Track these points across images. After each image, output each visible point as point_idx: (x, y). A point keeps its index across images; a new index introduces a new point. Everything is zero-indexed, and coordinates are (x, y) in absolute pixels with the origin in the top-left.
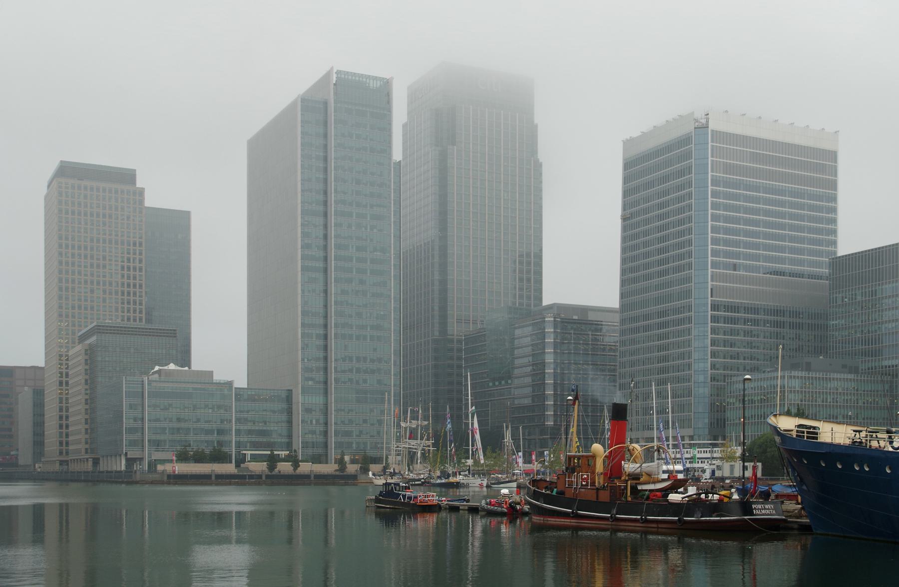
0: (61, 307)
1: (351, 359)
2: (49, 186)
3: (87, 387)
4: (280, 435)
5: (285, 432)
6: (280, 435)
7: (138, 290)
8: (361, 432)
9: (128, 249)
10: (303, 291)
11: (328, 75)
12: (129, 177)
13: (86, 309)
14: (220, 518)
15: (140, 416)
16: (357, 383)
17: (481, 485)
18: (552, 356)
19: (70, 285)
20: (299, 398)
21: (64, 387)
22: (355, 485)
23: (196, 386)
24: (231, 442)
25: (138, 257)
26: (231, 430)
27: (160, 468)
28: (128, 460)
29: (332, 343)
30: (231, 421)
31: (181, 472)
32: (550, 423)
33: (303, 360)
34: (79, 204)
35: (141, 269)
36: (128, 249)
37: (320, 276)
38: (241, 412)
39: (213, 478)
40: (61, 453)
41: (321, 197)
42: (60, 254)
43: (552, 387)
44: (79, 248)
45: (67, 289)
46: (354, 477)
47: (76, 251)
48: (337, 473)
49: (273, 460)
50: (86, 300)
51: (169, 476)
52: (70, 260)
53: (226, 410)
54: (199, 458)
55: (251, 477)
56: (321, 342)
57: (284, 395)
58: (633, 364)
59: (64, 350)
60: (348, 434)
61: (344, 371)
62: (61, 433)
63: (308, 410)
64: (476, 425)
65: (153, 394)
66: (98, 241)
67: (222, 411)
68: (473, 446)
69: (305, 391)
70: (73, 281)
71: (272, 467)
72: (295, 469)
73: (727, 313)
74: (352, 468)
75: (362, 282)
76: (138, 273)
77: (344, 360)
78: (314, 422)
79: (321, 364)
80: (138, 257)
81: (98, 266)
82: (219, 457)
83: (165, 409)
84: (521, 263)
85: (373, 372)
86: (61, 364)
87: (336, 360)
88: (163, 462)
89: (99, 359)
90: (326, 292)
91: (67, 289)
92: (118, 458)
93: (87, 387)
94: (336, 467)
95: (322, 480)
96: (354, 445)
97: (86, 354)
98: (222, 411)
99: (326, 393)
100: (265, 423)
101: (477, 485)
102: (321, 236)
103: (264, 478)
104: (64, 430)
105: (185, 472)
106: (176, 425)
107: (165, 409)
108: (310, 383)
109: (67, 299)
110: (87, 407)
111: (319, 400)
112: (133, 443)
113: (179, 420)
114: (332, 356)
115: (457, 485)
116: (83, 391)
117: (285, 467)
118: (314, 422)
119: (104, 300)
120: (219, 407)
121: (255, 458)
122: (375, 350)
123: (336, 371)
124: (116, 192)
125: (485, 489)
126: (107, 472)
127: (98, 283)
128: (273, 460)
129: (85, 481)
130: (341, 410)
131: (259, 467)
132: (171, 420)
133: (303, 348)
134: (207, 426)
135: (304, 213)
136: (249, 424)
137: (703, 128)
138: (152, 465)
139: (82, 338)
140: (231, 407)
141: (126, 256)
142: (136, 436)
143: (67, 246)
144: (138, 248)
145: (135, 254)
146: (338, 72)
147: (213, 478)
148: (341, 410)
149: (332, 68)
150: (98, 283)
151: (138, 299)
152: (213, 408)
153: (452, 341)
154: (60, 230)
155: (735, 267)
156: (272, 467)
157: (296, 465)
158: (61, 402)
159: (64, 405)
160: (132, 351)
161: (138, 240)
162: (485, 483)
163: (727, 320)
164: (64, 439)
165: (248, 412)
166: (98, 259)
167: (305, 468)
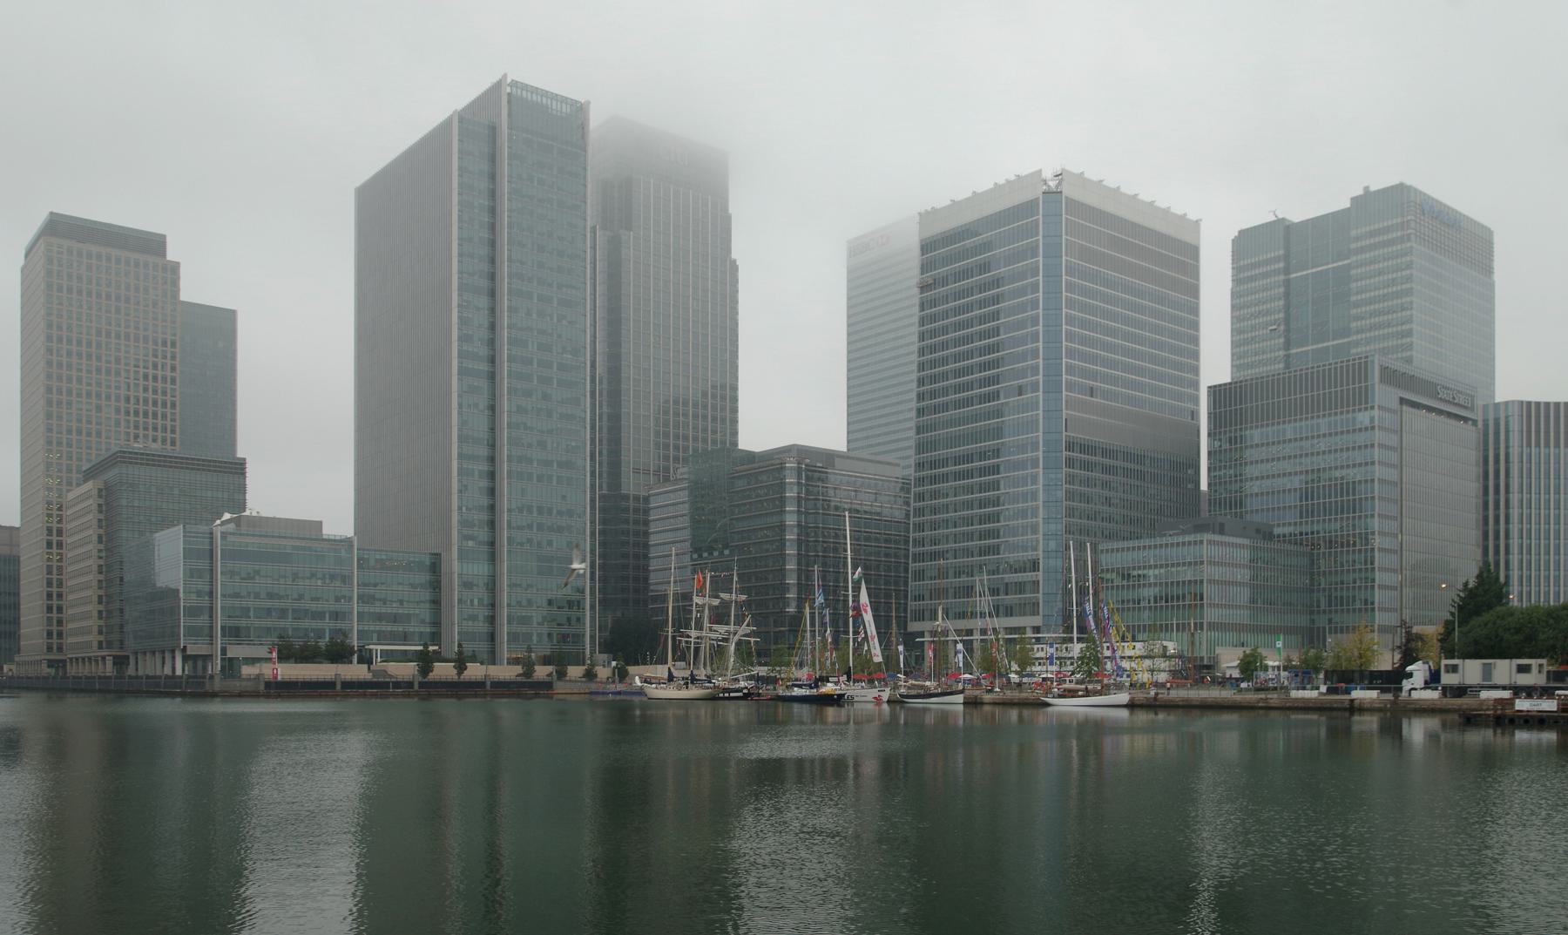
0: (50, 430)
1: (530, 510)
2: (27, 256)
3: (102, 547)
4: (423, 621)
5: (427, 616)
6: (423, 621)
7: (169, 410)
9: (155, 350)
10: (460, 406)
11: (497, 86)
12: (153, 245)
13: (89, 434)
15: (207, 588)
16: (539, 544)
17: (878, 700)
18: (795, 517)
19: (64, 398)
20: (455, 567)
21: (55, 550)
22: (550, 697)
23: (298, 543)
24: (351, 630)
25: (169, 362)
27: (247, 670)
28: (186, 658)
29: (504, 487)
30: (351, 599)
31: (287, 678)
32: (792, 609)
33: (460, 508)
34: (80, 279)
35: (173, 381)
36: (155, 350)
37: (483, 384)
38: (365, 585)
39: (339, 687)
40: (50, 649)
41: (485, 267)
42: (50, 350)
43: (795, 560)
44: (79, 343)
45: (60, 403)
46: (547, 685)
47: (74, 348)
49: (425, 661)
50: (89, 422)
51: (268, 685)
52: (65, 360)
54: (307, 655)
55: (397, 685)
56: (484, 483)
58: (935, 526)
59: (54, 495)
60: (525, 621)
61: (519, 528)
62: (50, 620)
63: (467, 585)
64: (864, 598)
65: (229, 555)
66: (108, 335)
68: (856, 633)
69: (463, 555)
70: (69, 392)
71: (425, 669)
72: (459, 674)
73: (1083, 455)
74: (542, 672)
75: (546, 397)
76: (169, 386)
77: (521, 510)
79: (485, 516)
80: (169, 362)
81: (108, 372)
82: (339, 654)
83: (249, 577)
84: (714, 396)
85: (560, 529)
86: (49, 516)
87: (509, 510)
88: (252, 661)
89: (124, 502)
90: (492, 408)
91: (60, 403)
92: (158, 656)
93: (102, 547)
94: (519, 669)
95: (502, 688)
97: (100, 496)
98: (338, 584)
99: (493, 558)
100: (401, 602)
101: (870, 698)
102: (486, 324)
103: (416, 686)
104: (55, 615)
105: (293, 678)
106: (269, 604)
107: (249, 577)
108: (471, 543)
109: (60, 418)
110: (101, 577)
111: (480, 569)
112: (193, 632)
113: (271, 596)
114: (505, 503)
115: (836, 700)
116: (95, 553)
117: (443, 671)
119: (118, 424)
120: (333, 577)
121: (389, 656)
122: (564, 497)
124: (137, 265)
125: (885, 706)
126: (148, 677)
127: (108, 398)
128: (425, 661)
129: (100, 691)
131: (406, 670)
132: (257, 596)
133: (460, 491)
134: (313, 606)
135: (462, 288)
136: (378, 604)
137: (1052, 196)
138: (231, 666)
139: (89, 475)
140: (351, 578)
141: (151, 359)
142: (203, 620)
143: (60, 340)
144: (169, 349)
145: (165, 357)
146: (514, 84)
147: (339, 687)
149: (505, 76)
150: (108, 398)
151: (169, 423)
152: (323, 578)
153: (626, 497)
154: (49, 314)
155: (1092, 392)
156: (425, 669)
157: (461, 667)
158: (50, 573)
159: (55, 577)
160: (176, 491)
161: (169, 338)
162: (885, 696)
163: (1087, 466)
164: (55, 629)
165: (375, 585)
166: (109, 362)
167: (475, 671)
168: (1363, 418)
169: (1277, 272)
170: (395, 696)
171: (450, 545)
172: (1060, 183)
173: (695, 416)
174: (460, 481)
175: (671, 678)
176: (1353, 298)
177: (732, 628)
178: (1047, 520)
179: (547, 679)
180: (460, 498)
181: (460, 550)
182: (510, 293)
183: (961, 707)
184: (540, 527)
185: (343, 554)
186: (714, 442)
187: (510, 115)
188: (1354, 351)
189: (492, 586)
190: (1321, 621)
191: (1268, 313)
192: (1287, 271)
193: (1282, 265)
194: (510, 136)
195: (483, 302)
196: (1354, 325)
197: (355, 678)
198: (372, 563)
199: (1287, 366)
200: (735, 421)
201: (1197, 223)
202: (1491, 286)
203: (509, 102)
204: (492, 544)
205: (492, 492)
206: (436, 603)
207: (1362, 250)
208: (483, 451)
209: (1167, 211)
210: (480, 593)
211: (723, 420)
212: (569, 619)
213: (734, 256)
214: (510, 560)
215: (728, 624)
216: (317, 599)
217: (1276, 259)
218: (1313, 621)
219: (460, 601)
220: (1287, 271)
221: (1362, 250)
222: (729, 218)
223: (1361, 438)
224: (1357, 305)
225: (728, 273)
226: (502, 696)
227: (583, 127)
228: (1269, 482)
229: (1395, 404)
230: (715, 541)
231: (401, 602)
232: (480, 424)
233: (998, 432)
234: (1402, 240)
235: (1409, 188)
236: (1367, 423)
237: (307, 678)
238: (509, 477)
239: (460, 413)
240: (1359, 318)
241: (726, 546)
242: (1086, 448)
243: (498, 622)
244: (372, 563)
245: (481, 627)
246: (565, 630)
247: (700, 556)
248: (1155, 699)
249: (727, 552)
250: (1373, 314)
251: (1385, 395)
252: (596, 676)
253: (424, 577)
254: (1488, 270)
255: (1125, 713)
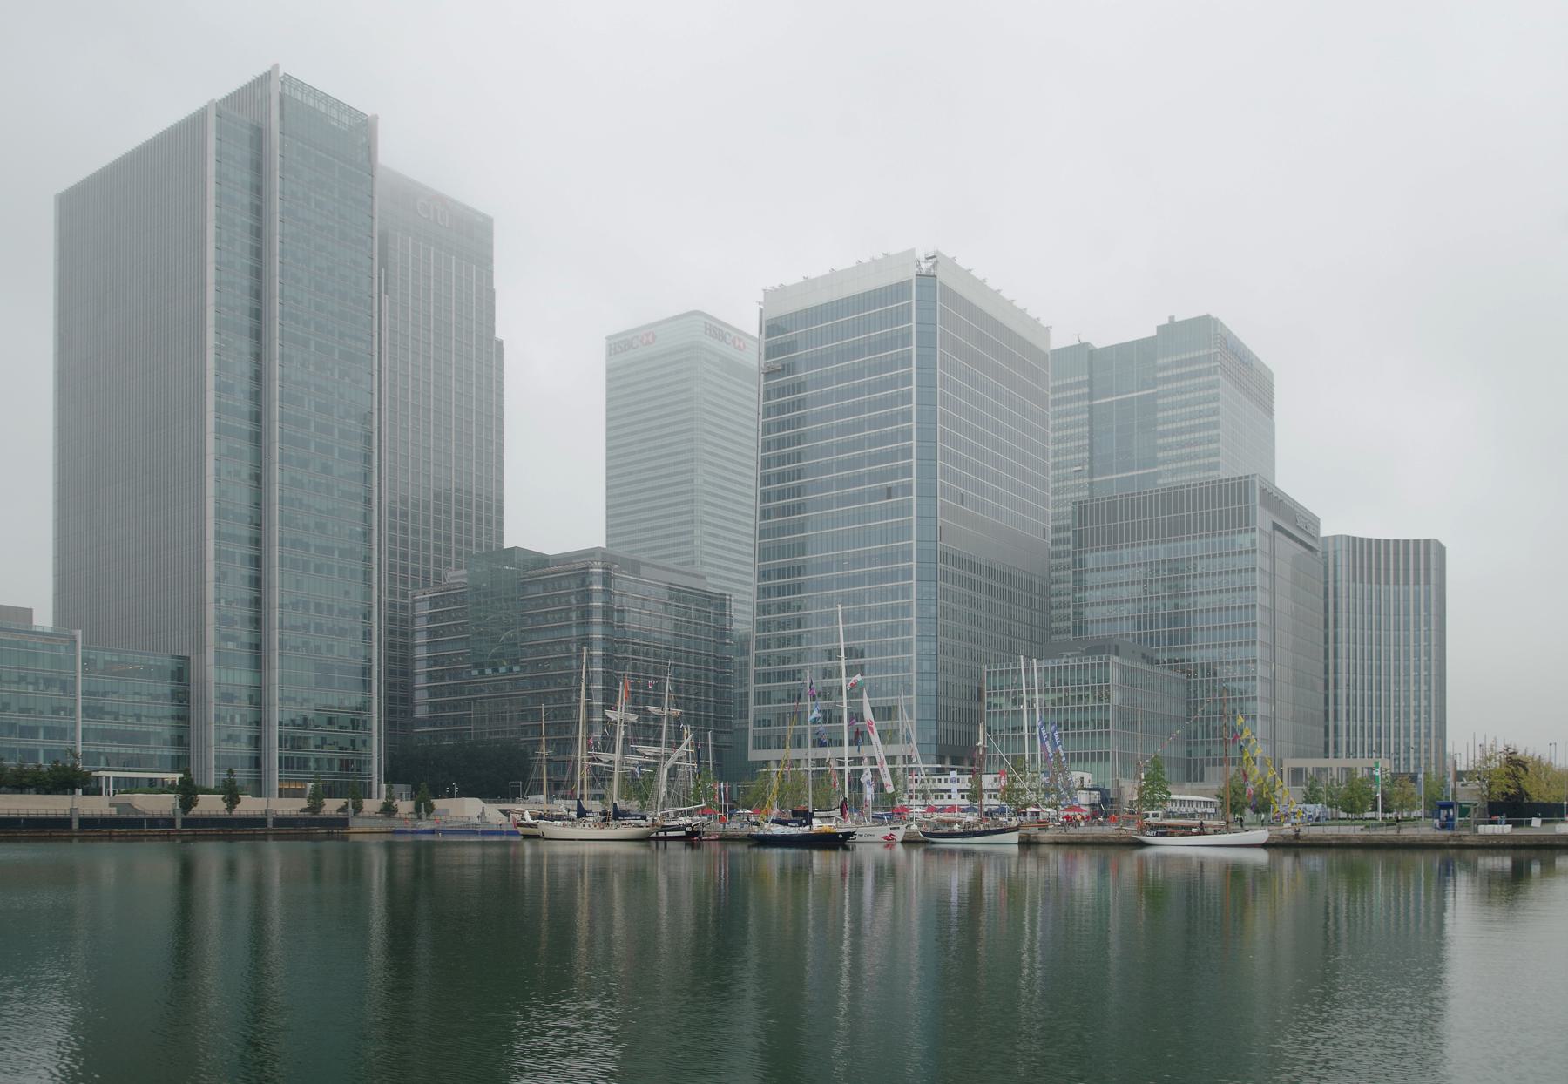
1: (306, 608)
8: (324, 740)
10: (218, 472)
11: (266, 78)
14: (952, 852)
16: (318, 649)
17: (889, 841)
26: (74, 729)
30: (72, 711)
33: (218, 600)
37: (245, 446)
39: (75, 825)
48: (308, 815)
53: (64, 689)
55: (153, 822)
56: (246, 571)
57: (168, 663)
60: (297, 742)
61: (294, 628)
63: (227, 697)
67: (56, 690)
71: (187, 803)
74: (331, 806)
75: (326, 469)
77: (295, 606)
78: (237, 719)
82: (65, 780)
87: (282, 606)
96: (312, 764)
98: (56, 690)
99: (258, 661)
100: (138, 717)
101: (878, 837)
103: (178, 825)
105: (13, 813)
108: (231, 645)
114: (275, 596)
117: (210, 805)
118: (237, 719)
120: (49, 682)
123: (282, 627)
128: (188, 792)
130: (289, 699)
131: (165, 804)
133: (218, 579)
134: (23, 720)
136: (107, 718)
146: (287, 79)
147: (75, 825)
148: (289, 699)
149: (276, 67)
152: (36, 683)
156: (187, 803)
157: (233, 800)
162: (899, 835)
165: (105, 694)
167: (249, 805)
168: (1243, 540)
169: (1080, 398)
170: (151, 837)
171: (203, 649)
172: (934, 266)
173: (458, 515)
174: (218, 566)
175: (582, 813)
176: (1160, 428)
177: (663, 749)
178: (921, 637)
179: (341, 815)
180: (218, 588)
181: (218, 652)
182: (282, 337)
183: (1016, 848)
184: (319, 628)
185: (63, 652)
186: (479, 545)
187: (282, 117)
188: (1160, 481)
189: (257, 699)
190: (1199, 753)
191: (1070, 438)
192: (1091, 397)
193: (1086, 390)
194: (283, 142)
195: (245, 345)
196: (1160, 455)
197: (97, 814)
198: (100, 665)
199: (1091, 495)
200: (500, 523)
201: (1047, 329)
202: (1272, 427)
203: (282, 102)
204: (257, 646)
205: (257, 582)
206: (182, 718)
207: (1166, 380)
208: (245, 531)
209: (1023, 312)
210: (242, 709)
211: (489, 522)
212: (353, 742)
213: (498, 335)
214: (282, 667)
215: (657, 743)
216: (28, 710)
217: (1079, 385)
218: (1189, 753)
219: (218, 717)
220: (1091, 397)
221: (1166, 380)
222: (492, 293)
223: (1241, 562)
224: (1164, 435)
225: (488, 357)
226: (207, 838)
227: (370, 150)
228: (1217, 597)
229: (1269, 528)
230: (501, 655)
231: (138, 717)
232: (241, 497)
233: (801, 548)
234: (1208, 372)
235: (1216, 321)
236: (1248, 546)
237: (33, 813)
238: (282, 564)
239: (218, 481)
240: (1164, 448)
241: (517, 662)
242: (958, 561)
243: (265, 742)
244: (100, 665)
245: (243, 750)
246: (348, 755)
247: (482, 673)
248: (1297, 836)
249: (516, 668)
250: (1181, 445)
251: (1263, 518)
252: (395, 811)
253: (166, 687)
254: (1270, 412)
255: (1262, 857)
